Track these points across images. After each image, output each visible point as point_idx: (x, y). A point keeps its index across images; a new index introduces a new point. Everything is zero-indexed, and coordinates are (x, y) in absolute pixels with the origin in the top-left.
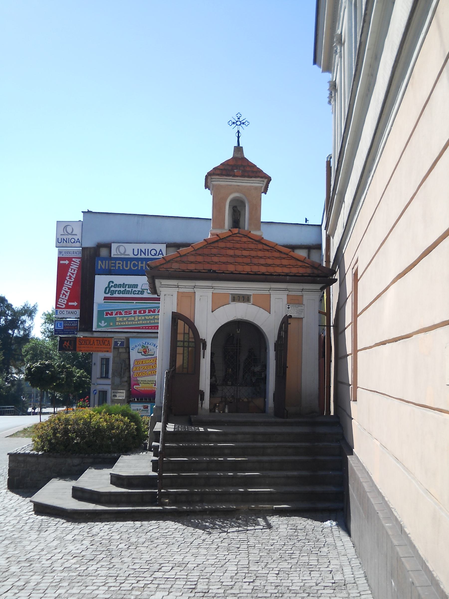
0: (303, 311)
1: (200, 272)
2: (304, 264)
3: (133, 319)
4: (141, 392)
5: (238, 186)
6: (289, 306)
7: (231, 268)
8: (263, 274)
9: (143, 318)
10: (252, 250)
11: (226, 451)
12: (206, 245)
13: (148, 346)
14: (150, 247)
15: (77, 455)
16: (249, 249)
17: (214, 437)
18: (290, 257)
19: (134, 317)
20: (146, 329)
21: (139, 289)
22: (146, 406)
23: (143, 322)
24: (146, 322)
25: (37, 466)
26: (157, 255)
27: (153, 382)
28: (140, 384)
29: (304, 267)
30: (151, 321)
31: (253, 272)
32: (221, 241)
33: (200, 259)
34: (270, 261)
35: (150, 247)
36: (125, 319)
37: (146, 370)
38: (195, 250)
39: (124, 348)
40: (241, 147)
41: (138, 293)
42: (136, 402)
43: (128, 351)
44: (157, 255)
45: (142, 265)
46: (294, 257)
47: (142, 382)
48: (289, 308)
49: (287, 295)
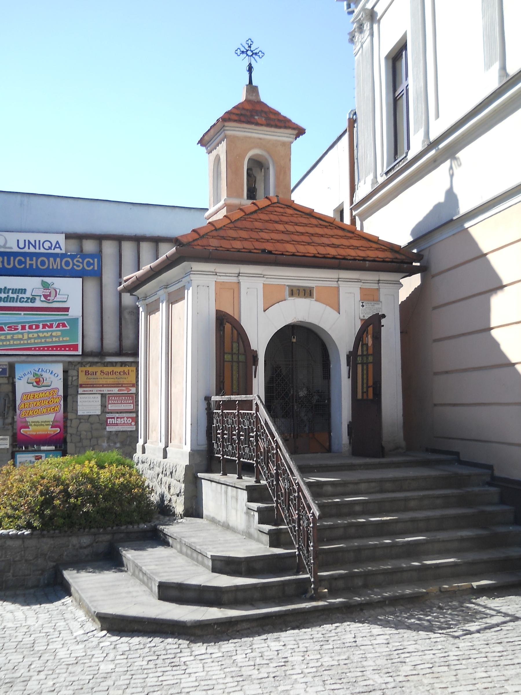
3: (20, 336)
4: (31, 437)
5: (260, 139)
6: (363, 303)
7: (291, 248)
8: (334, 258)
9: (36, 335)
10: (306, 225)
11: (358, 508)
12: (244, 217)
13: (43, 373)
14: (42, 237)
15: (87, 530)
16: (303, 225)
17: (329, 489)
19: (22, 334)
20: (39, 350)
21: (28, 295)
22: (39, 456)
23: (36, 341)
24: (40, 341)
25: (23, 553)
26: (53, 248)
27: (48, 423)
28: (30, 427)
30: (48, 340)
31: (321, 254)
33: (244, 234)
35: (42, 237)
36: (9, 337)
37: (40, 407)
38: (231, 222)
39: (6, 377)
40: (256, 86)
41: (27, 300)
42: (23, 451)
43: (11, 381)
44: (53, 248)
45: (31, 262)
46: (364, 236)
47: (34, 424)
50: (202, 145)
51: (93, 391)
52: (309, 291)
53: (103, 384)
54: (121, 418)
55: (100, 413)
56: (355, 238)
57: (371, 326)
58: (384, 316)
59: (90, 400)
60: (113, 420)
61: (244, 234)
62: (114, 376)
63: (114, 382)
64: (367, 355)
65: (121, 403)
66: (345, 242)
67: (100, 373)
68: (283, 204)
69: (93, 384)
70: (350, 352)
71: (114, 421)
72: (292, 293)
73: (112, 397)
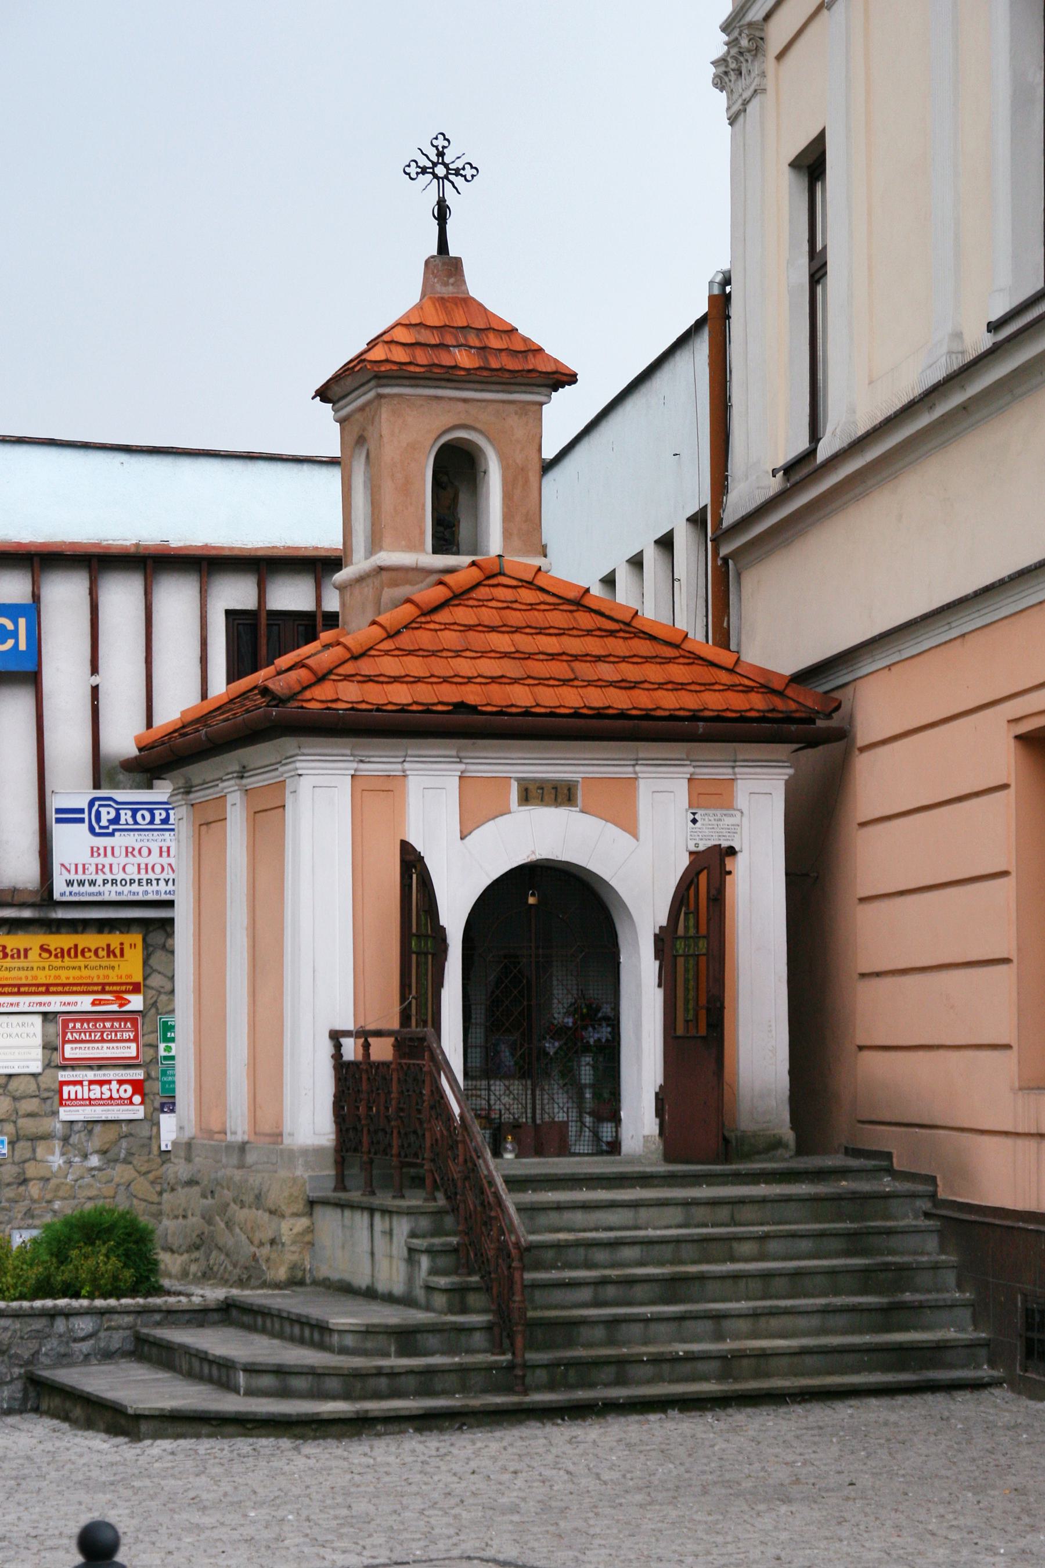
0: (739, 831)
1: (429, 711)
2: (737, 680)
6: (694, 814)
7: (521, 697)
10: (562, 633)
18: (687, 654)
29: (740, 688)
32: (456, 602)
33: (415, 666)
34: (631, 672)
40: (456, 258)
48: (694, 821)
49: (352, 776)
50: (325, 399)
51: (18, 1004)
52: (566, 791)
53: (48, 985)
54: (101, 1083)
55: (39, 1070)
56: (681, 660)
57: (705, 871)
58: (731, 851)
59: (9, 1030)
60: (78, 1088)
61: (415, 666)
62: (80, 961)
63: (81, 977)
64: (697, 938)
65: (103, 1041)
66: (653, 673)
67: (39, 951)
68: (514, 578)
69: (19, 986)
70: (661, 928)
71: (82, 1092)
72: (526, 798)
73: (75, 1021)
